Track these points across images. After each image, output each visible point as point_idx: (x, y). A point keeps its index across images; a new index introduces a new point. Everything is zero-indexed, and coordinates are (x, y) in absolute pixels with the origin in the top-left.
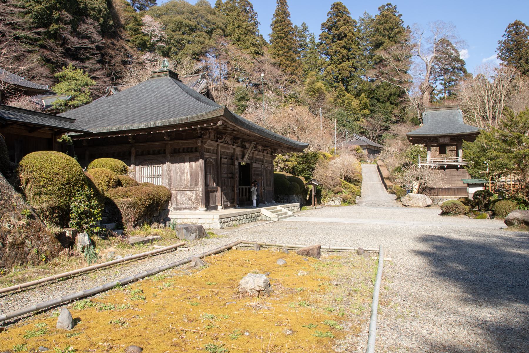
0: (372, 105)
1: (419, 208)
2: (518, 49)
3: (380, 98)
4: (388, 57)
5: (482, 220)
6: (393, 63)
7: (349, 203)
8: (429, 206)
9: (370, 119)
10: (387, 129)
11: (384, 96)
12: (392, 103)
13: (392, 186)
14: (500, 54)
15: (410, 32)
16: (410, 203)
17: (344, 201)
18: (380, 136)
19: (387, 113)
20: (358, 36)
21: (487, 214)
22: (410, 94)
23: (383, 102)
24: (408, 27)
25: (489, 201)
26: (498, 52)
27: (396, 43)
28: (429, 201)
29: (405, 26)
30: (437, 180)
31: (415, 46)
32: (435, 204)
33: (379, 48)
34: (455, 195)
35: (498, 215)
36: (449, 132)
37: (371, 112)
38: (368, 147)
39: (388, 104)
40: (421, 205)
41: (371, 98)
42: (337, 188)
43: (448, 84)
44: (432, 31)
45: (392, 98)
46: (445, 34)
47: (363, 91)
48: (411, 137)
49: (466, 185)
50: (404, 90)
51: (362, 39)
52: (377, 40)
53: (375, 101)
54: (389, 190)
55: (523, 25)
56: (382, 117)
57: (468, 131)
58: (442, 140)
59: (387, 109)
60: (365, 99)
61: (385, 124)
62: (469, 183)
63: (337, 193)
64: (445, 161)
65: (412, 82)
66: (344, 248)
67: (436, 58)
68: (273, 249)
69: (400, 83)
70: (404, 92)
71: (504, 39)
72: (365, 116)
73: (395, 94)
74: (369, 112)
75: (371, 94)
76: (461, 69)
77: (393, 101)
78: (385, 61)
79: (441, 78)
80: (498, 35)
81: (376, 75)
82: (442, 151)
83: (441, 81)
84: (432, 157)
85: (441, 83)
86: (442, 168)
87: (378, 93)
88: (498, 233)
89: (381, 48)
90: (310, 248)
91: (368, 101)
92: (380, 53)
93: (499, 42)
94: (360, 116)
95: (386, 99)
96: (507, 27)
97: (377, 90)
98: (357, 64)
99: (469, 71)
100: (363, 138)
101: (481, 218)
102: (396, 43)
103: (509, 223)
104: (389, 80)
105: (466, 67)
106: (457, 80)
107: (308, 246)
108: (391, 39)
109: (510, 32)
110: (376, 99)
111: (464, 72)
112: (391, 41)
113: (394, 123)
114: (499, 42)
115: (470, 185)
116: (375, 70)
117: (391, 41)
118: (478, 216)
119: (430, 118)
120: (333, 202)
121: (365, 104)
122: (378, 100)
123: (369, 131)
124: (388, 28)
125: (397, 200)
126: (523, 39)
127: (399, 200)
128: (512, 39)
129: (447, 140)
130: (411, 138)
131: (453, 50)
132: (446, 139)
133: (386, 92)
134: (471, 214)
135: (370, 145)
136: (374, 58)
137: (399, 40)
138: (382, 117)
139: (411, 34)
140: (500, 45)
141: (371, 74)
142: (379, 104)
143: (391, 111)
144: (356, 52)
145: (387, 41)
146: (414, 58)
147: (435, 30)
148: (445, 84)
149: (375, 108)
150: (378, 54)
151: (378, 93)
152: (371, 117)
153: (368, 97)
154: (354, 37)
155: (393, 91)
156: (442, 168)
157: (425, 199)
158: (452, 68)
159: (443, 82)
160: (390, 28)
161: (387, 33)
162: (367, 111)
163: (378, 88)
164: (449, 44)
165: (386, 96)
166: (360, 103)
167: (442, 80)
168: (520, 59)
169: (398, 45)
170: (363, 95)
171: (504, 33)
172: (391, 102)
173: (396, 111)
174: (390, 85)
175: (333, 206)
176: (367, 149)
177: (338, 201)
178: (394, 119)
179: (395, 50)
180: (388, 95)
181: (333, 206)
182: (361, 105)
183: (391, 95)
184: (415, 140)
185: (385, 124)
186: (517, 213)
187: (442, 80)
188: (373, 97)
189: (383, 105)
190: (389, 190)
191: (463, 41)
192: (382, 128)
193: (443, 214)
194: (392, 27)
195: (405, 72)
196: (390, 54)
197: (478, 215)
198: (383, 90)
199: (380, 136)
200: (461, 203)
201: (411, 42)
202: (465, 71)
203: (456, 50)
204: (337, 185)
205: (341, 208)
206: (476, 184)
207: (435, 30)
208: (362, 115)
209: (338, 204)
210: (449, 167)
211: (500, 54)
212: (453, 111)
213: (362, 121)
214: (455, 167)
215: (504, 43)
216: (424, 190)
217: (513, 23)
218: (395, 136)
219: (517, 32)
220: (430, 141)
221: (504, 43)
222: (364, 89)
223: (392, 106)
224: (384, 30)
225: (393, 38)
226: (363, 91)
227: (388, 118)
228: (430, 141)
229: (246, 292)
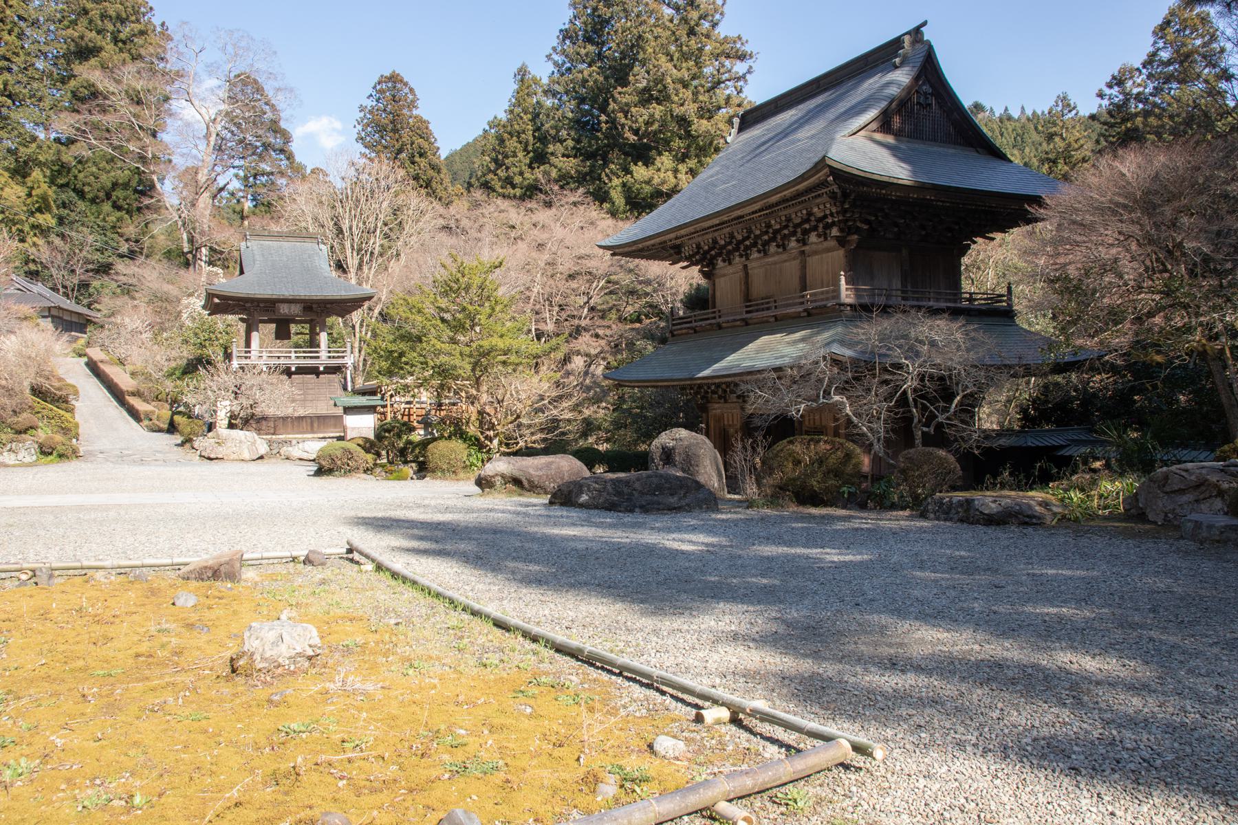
0: (64, 205)
1: (243, 464)
2: (395, 131)
3: (87, 189)
4: (111, 89)
5: (403, 482)
6: (126, 109)
7: (61, 456)
8: (261, 457)
9: (58, 241)
10: (104, 269)
11: (97, 186)
12: (117, 207)
13: (153, 412)
14: (363, 134)
15: (170, 38)
16: (220, 452)
17: (45, 451)
18: (84, 285)
19: (103, 228)
20: (22, 12)
21: (409, 470)
22: (169, 191)
23: (93, 201)
24: (163, 24)
25: (409, 442)
26: (360, 128)
27: (133, 59)
28: (263, 448)
29: (157, 21)
30: (279, 399)
31: (179, 74)
32: (275, 452)
33: (87, 59)
34: (313, 432)
35: (433, 471)
36: (304, 292)
37: (61, 221)
38: (54, 312)
39: (107, 207)
40: (246, 456)
41: (61, 186)
42: (25, 418)
43: (251, 179)
44: (224, 49)
45: (118, 193)
46: (252, 65)
47: (40, 164)
48: (218, 296)
49: (340, 411)
50: (152, 181)
51: (35, 23)
52: (82, 37)
53: (72, 194)
54: (146, 422)
55: (406, 84)
56: (91, 239)
57: (343, 293)
58: (284, 309)
59: (104, 220)
60: (45, 186)
61: (97, 256)
62: (347, 405)
63: (25, 431)
64: (293, 355)
65: (170, 161)
66: (266, 555)
67: (227, 114)
68: (99, 575)
69: (143, 159)
70: (153, 187)
71: (370, 103)
72: (43, 231)
73: (126, 186)
74: (53, 222)
75: (59, 172)
76: (282, 151)
77: (121, 202)
78: (105, 98)
79: (237, 163)
80: (359, 95)
81: (78, 129)
82: (282, 333)
83: (235, 171)
84: (263, 349)
85: (236, 176)
86: (288, 372)
87: (81, 176)
88: (460, 503)
89: (93, 61)
90: (223, 560)
91: (50, 192)
92: (88, 73)
93: (362, 108)
94: (27, 228)
95: (102, 194)
96: (376, 80)
97: (80, 167)
98: (18, 89)
99: (299, 158)
100: (38, 288)
101: (399, 478)
102: (133, 59)
103: (484, 483)
104: (114, 149)
105: (294, 147)
106: (272, 173)
107: (205, 557)
108: (120, 44)
109: (381, 92)
110: (74, 190)
111: (288, 159)
112: (121, 50)
113: (121, 256)
114: (362, 108)
115: (349, 410)
116: (77, 117)
117: (121, 50)
118: (390, 473)
119: (257, 257)
120: (13, 456)
121: (44, 198)
122: (81, 194)
123: (54, 271)
124: (114, 14)
125: (182, 444)
126: (405, 111)
127: (188, 445)
128: (386, 106)
129: (296, 309)
130: (216, 300)
131: (266, 104)
132: (293, 306)
133: (104, 177)
134: (378, 470)
135: (60, 308)
136: (73, 83)
137: (143, 52)
138: (91, 239)
139: (171, 45)
140: (362, 114)
141: (64, 124)
142: (81, 205)
143: (114, 227)
144: (17, 55)
145: (110, 47)
146: (177, 104)
147: (230, 49)
148: (246, 178)
149: (73, 214)
150: (85, 76)
151: (81, 176)
152: (62, 236)
153: (52, 182)
154: (8, 12)
155: (122, 176)
156: (288, 372)
157: (254, 443)
158: (263, 145)
159: (242, 174)
160: (119, 17)
161: (110, 27)
162: (47, 219)
163: (80, 162)
164: (259, 90)
165: (103, 188)
166: (30, 195)
167: (239, 167)
168: (400, 151)
169: (139, 64)
170: (36, 174)
171: (370, 91)
172: (114, 202)
173: (131, 230)
174: (112, 160)
175: (14, 466)
176: (53, 317)
177: (26, 451)
178: (124, 248)
179: (131, 76)
180: (109, 185)
181: (14, 466)
182: (29, 201)
183: (115, 185)
184: (220, 304)
185: (97, 256)
186: (501, 463)
187: (239, 167)
188: (67, 185)
189: (94, 208)
190: (146, 422)
191: (291, 90)
192: (90, 266)
193: (320, 472)
194: (124, 15)
195: (154, 135)
196: (118, 82)
197: (391, 472)
198: (94, 169)
199: (84, 285)
200: (359, 449)
201: (172, 64)
202: (290, 157)
203: (273, 105)
204: (23, 410)
205: (35, 469)
206: (356, 407)
207: (230, 49)
208: (33, 227)
209: (28, 459)
210: (302, 370)
211: (363, 134)
212: (310, 246)
213: (35, 244)
214: (314, 371)
215: (371, 112)
216: (243, 421)
217: (387, 74)
218: (127, 290)
219: (394, 96)
220: (256, 310)
221: (371, 112)
222: (41, 158)
223: (119, 214)
224: (103, 16)
225: (124, 42)
226: (40, 164)
227: (106, 243)
228: (256, 310)
229: (279, 666)
